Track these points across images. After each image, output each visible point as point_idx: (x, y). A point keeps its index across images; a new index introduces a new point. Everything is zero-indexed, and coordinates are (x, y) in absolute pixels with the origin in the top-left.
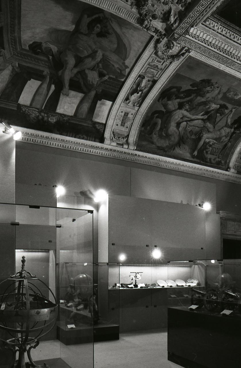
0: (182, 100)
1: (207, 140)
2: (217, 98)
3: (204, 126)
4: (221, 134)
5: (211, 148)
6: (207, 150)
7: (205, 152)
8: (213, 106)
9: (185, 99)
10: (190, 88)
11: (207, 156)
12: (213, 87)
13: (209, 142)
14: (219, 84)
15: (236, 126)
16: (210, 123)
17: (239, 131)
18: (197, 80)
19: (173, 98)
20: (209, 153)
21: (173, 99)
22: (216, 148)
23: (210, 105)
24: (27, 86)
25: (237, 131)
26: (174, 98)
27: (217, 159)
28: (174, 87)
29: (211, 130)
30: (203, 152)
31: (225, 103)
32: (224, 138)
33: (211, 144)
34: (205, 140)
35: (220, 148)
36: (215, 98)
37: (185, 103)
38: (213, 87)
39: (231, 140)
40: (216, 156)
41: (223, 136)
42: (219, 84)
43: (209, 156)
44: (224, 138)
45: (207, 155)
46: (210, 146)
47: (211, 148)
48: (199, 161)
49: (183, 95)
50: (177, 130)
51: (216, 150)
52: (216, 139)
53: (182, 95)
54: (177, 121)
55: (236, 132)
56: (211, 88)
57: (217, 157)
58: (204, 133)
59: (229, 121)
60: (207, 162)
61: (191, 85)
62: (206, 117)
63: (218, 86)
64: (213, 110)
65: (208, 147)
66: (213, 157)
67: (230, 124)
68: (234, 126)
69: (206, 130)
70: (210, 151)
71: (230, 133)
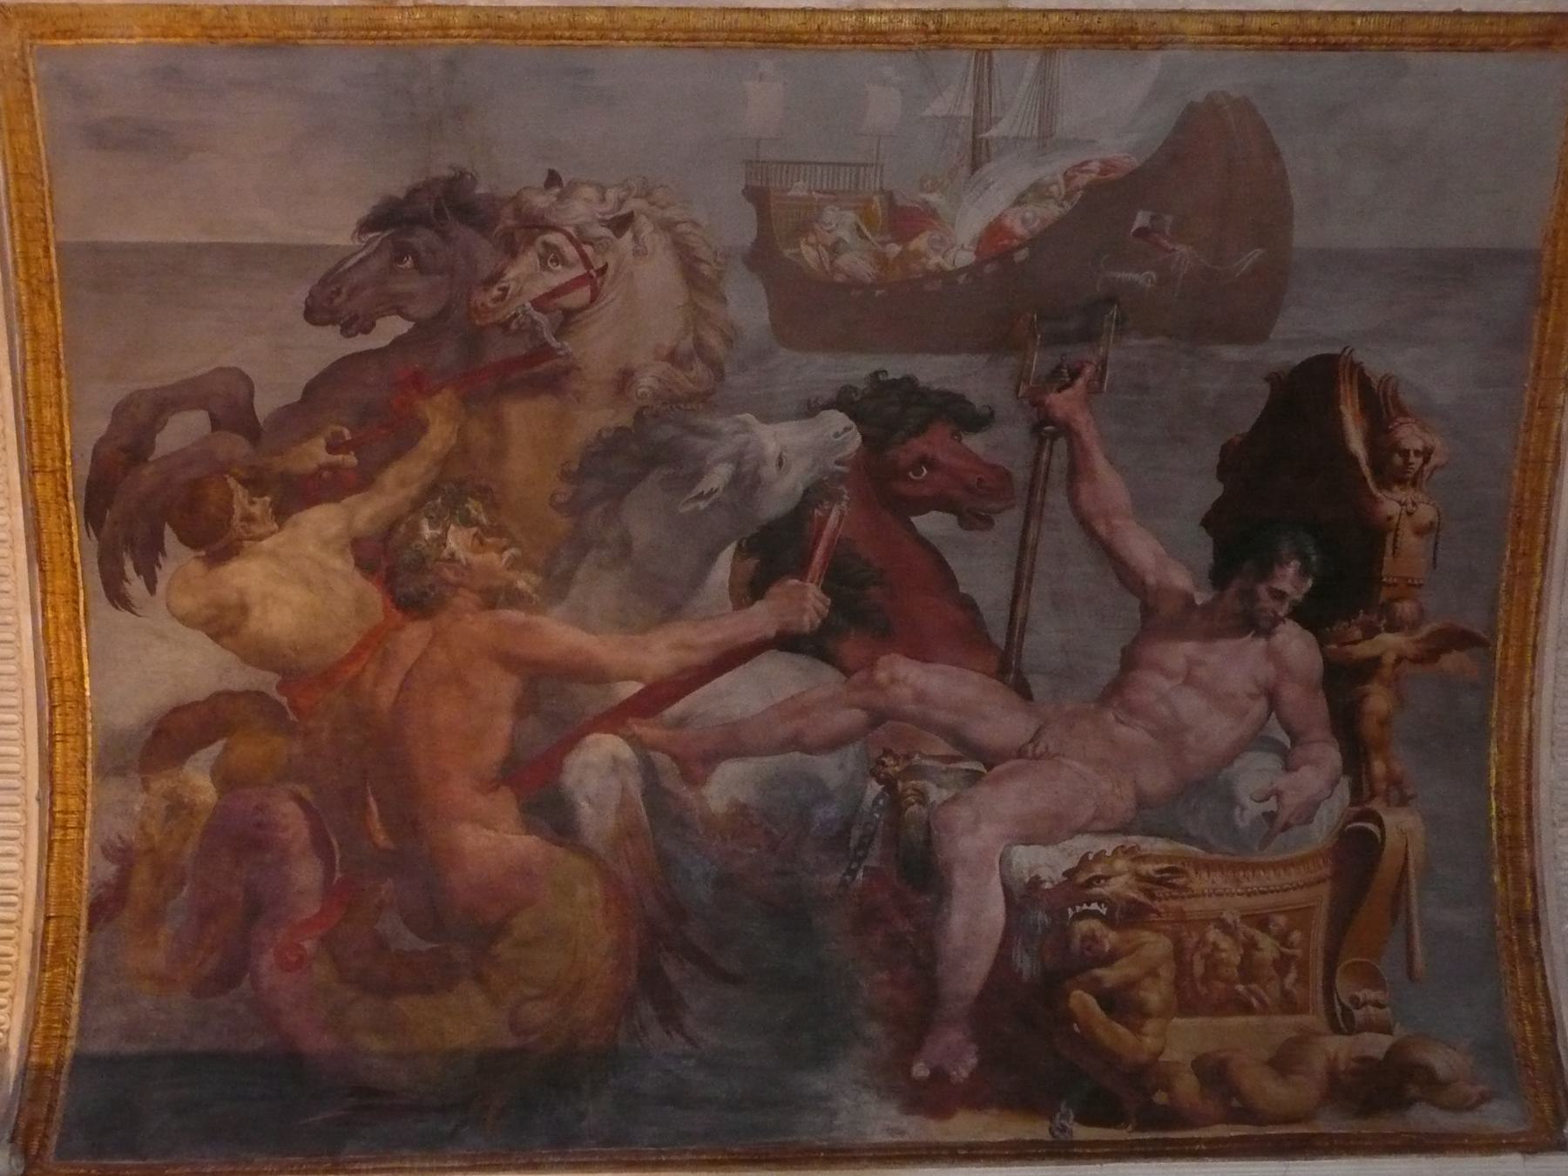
0: (366, 511)
1: (1046, 863)
2: (729, 341)
3: (878, 718)
4: (1171, 734)
5: (1155, 945)
6: (1110, 976)
7: (1082, 1000)
8: (772, 448)
9: (389, 477)
10: (330, 345)
11: (1149, 1042)
12: (554, 238)
13: (1078, 884)
14: (602, 189)
15: (1290, 580)
16: (920, 653)
17: (1392, 628)
18: (318, 237)
19: (249, 518)
20: (1154, 996)
21: (257, 530)
22: (1228, 917)
23: (726, 448)
24: (946, 515)
25: (1370, 632)
26: (256, 510)
27: (1338, 1047)
28: (166, 403)
29: (1002, 723)
30: (1070, 1017)
31: (896, 367)
32: (1255, 776)
33: (1120, 885)
34: (1005, 861)
35: (1301, 916)
36: (699, 344)
37: (427, 531)
38: (554, 238)
39: (1378, 767)
40: (1289, 1005)
41: (1229, 758)
42: (602, 189)
43: (1179, 1041)
44: (1255, 776)
45: (1137, 1030)
46: (1129, 915)
47: (1155, 945)
48: (1038, 1130)
49: (332, 448)
50: (559, 853)
51: (1251, 946)
52: (1147, 816)
53: (316, 453)
54: (494, 752)
55: (1364, 650)
56: (552, 256)
57: (1314, 1020)
58: (936, 795)
59: (1168, 556)
60: (1172, 1117)
61: (315, 313)
62: (805, 601)
63: (608, 209)
64: (815, 494)
65: (1110, 939)
66: (1242, 1037)
67: (1180, 579)
68: (1280, 596)
69: (943, 748)
70: (1153, 973)
71: (1291, 693)
